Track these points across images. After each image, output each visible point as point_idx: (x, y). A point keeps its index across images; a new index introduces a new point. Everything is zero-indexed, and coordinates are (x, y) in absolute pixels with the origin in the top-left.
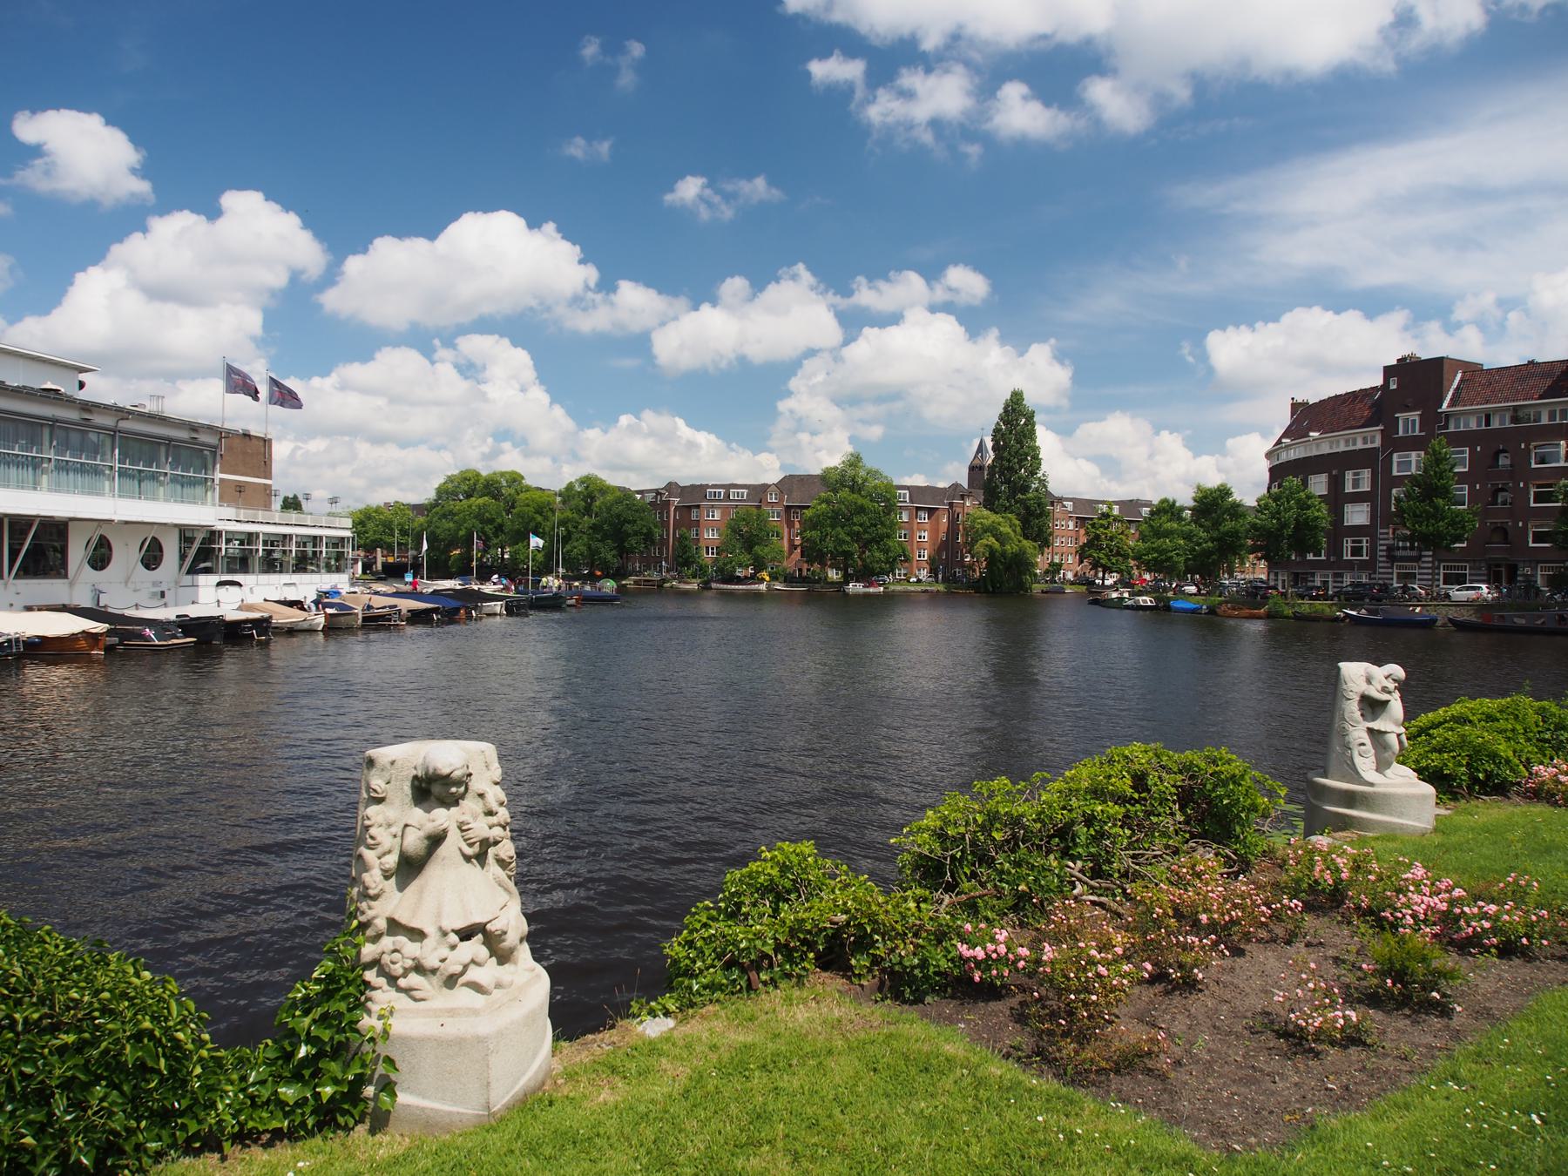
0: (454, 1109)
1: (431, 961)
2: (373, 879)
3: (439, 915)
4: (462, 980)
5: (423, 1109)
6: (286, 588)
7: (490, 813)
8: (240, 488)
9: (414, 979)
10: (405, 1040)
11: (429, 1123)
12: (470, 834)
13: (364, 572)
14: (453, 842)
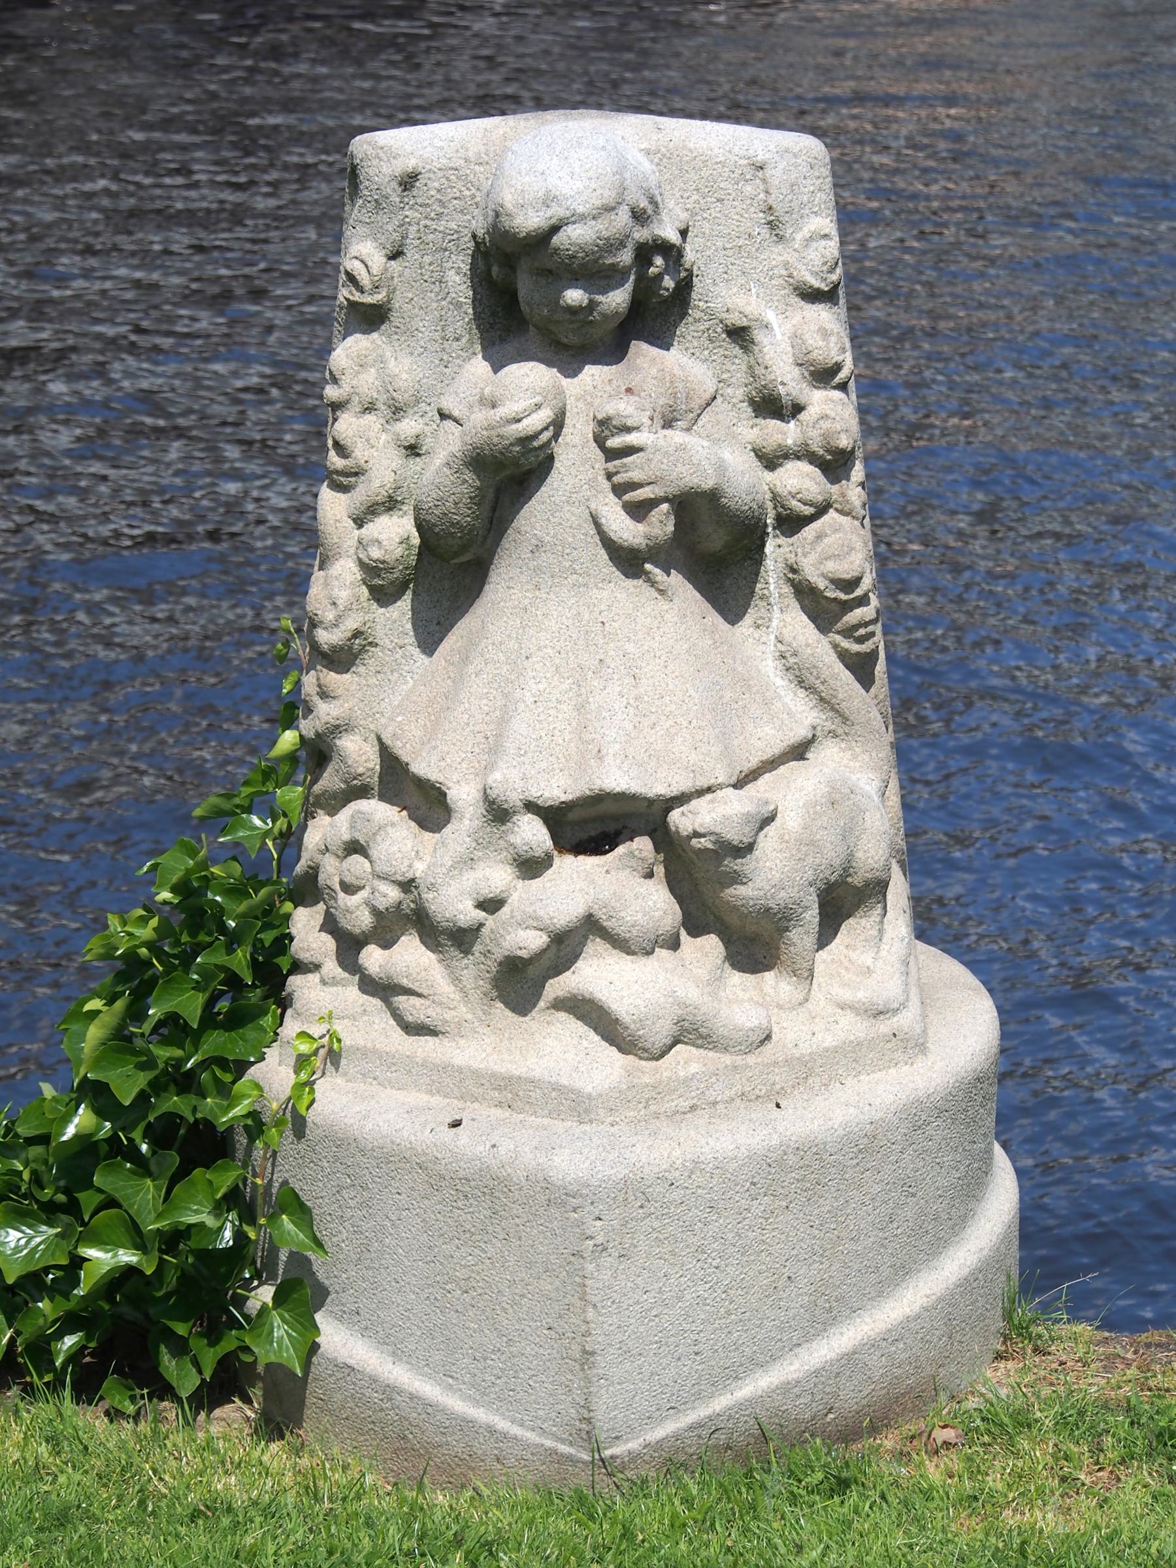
0: (481, 1415)
1: (454, 903)
2: (336, 594)
3: (494, 748)
4: (556, 987)
5: (390, 1390)
7: (770, 406)
9: (409, 957)
10: (344, 1146)
11: (413, 1447)
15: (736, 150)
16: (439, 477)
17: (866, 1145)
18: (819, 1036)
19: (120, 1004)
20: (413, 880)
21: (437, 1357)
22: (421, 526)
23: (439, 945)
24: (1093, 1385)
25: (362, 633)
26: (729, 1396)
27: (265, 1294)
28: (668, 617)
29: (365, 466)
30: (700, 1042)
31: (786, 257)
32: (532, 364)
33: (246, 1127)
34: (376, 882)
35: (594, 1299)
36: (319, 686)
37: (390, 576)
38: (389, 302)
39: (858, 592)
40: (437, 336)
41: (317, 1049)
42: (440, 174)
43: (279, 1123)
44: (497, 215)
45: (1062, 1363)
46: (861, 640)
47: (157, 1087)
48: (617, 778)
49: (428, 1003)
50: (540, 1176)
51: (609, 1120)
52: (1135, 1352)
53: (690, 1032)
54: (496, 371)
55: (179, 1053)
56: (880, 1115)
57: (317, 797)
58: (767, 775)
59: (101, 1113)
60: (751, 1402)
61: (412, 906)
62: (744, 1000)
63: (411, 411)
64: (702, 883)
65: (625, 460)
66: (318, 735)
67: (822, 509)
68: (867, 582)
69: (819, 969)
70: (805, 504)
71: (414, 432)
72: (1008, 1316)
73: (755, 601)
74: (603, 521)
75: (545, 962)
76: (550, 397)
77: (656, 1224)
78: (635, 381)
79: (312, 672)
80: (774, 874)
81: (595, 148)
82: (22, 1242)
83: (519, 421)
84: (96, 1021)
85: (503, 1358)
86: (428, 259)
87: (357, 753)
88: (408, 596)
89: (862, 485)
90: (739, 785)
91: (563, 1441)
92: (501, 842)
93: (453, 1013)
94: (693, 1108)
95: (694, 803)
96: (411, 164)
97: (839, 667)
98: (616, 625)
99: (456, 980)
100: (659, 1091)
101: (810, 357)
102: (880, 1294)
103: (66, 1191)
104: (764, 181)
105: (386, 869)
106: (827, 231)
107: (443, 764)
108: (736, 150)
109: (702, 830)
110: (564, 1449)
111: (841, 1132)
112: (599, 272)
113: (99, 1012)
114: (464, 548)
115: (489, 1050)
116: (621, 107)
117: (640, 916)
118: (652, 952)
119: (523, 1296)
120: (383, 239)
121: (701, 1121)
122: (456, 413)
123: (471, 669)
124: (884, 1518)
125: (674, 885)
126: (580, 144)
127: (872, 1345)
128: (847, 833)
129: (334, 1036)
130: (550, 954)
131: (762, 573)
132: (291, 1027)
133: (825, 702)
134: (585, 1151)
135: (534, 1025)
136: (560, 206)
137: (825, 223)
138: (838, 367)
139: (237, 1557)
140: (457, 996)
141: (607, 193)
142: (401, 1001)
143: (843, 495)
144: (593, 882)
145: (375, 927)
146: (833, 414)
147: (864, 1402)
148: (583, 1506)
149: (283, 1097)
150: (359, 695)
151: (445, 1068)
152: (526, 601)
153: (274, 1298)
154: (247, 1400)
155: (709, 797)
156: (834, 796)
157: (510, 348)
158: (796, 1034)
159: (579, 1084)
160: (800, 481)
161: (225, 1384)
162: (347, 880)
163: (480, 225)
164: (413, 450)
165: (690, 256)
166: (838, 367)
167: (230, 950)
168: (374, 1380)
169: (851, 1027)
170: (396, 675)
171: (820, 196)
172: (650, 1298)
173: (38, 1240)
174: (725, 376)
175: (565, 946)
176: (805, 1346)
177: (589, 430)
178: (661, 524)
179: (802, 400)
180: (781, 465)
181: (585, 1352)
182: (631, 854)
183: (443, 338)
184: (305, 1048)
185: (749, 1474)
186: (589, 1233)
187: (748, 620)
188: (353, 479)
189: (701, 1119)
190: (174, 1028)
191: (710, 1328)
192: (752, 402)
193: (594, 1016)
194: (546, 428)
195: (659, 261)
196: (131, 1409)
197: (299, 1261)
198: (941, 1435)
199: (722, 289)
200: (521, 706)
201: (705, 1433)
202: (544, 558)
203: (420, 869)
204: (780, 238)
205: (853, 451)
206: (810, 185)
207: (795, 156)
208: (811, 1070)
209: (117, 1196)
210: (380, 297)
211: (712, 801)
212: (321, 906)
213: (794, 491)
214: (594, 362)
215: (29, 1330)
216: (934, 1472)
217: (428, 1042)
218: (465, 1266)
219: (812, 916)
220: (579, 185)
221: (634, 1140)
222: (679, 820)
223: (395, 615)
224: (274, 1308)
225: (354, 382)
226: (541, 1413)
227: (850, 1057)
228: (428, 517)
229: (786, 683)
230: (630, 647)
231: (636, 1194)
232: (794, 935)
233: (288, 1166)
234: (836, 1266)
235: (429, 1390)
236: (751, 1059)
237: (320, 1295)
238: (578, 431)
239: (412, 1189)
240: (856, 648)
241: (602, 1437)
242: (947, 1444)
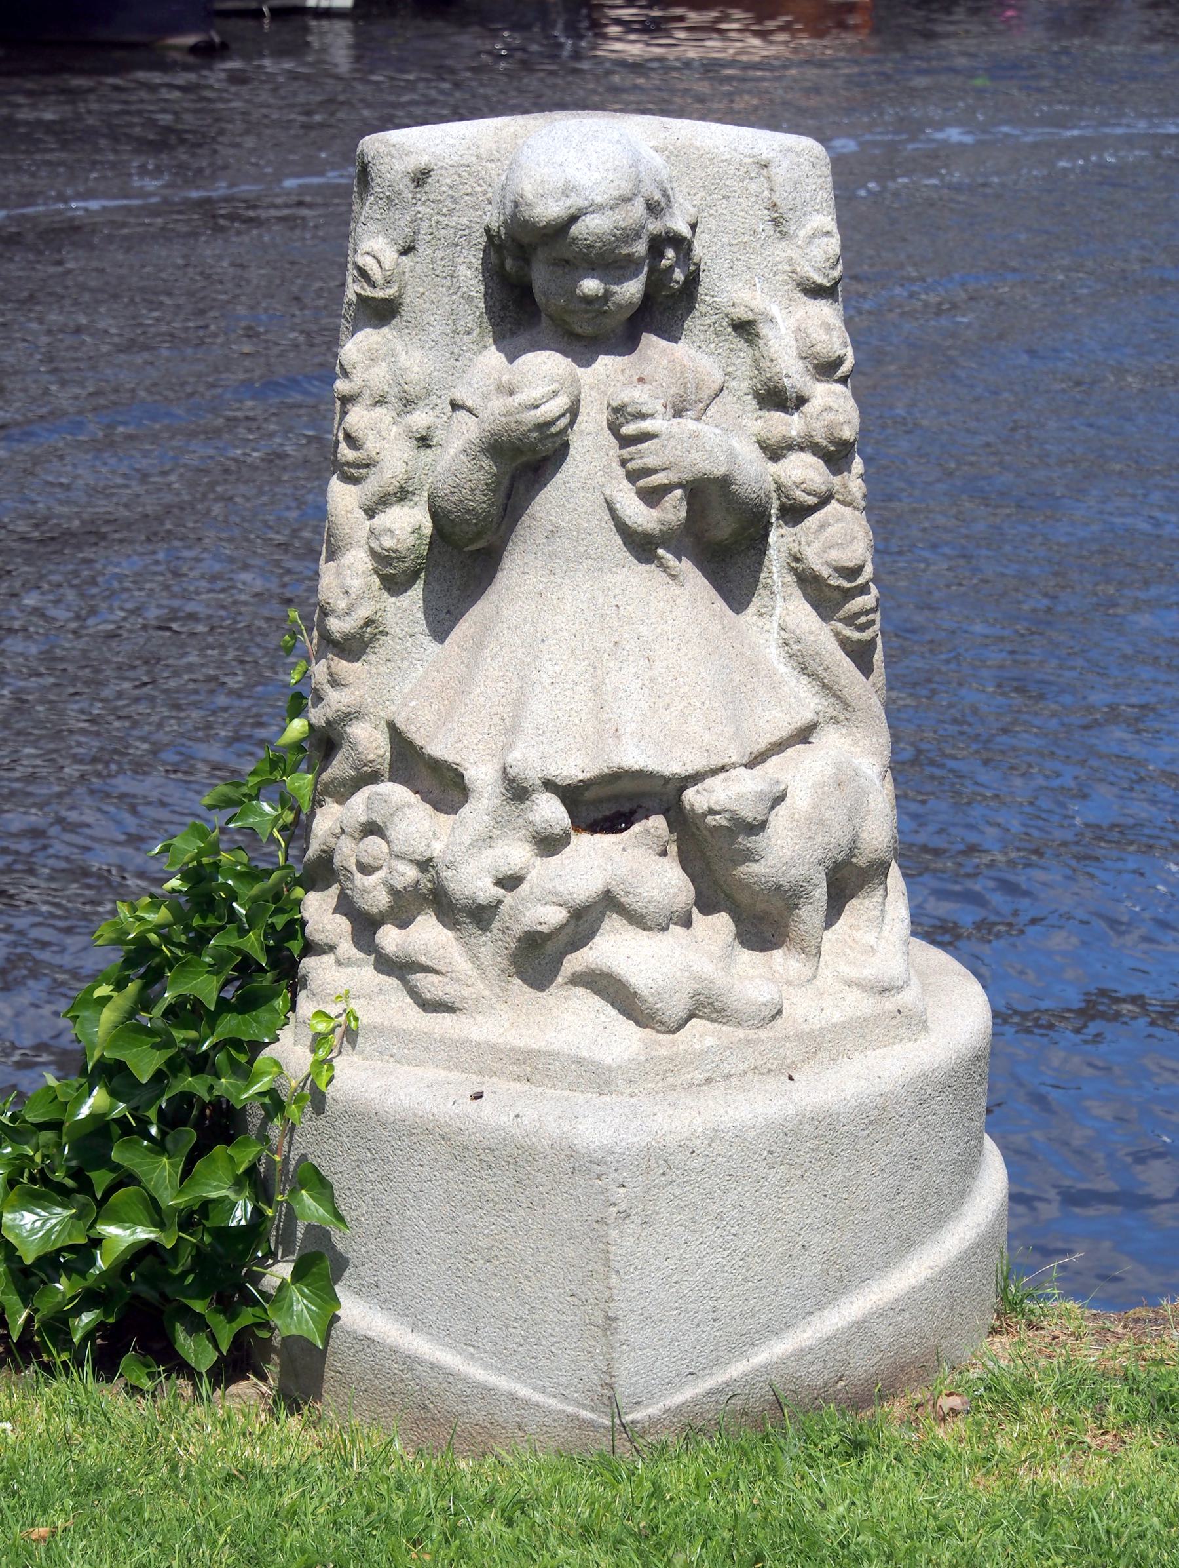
0: (503, 1383)
1: (473, 881)
3: (512, 730)
4: (574, 962)
5: (410, 1361)
7: (775, 398)
9: (426, 935)
10: (365, 1122)
11: (437, 1418)
14: (589, 473)
15: (741, 148)
16: (457, 463)
17: (876, 1117)
18: (828, 1012)
19: (132, 988)
20: (431, 860)
21: (459, 1326)
22: (436, 514)
23: (457, 922)
24: (1090, 1356)
25: (373, 621)
26: (745, 1362)
27: (283, 1270)
28: (679, 601)
29: (376, 458)
31: (790, 253)
32: (548, 353)
33: (263, 1105)
34: (394, 862)
35: (617, 1265)
36: (330, 674)
37: (402, 565)
38: (400, 296)
39: (861, 580)
40: (448, 330)
41: (334, 1029)
42: (452, 171)
43: (298, 1100)
44: (516, 205)
45: (1054, 1338)
46: (862, 628)
47: (173, 1067)
48: (634, 756)
49: (446, 980)
50: (565, 1144)
51: (628, 1091)
52: (1125, 1327)
53: (706, 1006)
54: (511, 361)
55: (193, 1034)
57: (326, 785)
58: (774, 758)
59: (114, 1094)
60: (766, 1368)
61: (429, 885)
62: (754, 976)
63: (422, 404)
64: (715, 859)
65: (640, 447)
66: (328, 722)
67: (825, 499)
68: (868, 571)
69: (825, 947)
71: (425, 424)
72: (1003, 1292)
73: (760, 590)
74: (618, 506)
75: (563, 938)
76: (567, 384)
77: (678, 1192)
78: (647, 370)
79: (323, 661)
80: (786, 852)
81: (610, 141)
82: (38, 1224)
83: (537, 407)
84: (110, 1005)
85: (525, 1326)
87: (368, 740)
88: (419, 586)
89: (861, 476)
90: (751, 764)
91: (585, 1407)
92: (520, 820)
93: (471, 990)
94: (708, 1081)
95: (709, 782)
96: (423, 160)
97: (841, 655)
98: (630, 608)
99: (474, 958)
100: (676, 1063)
101: (814, 350)
102: (887, 1265)
103: (83, 1171)
104: (768, 178)
105: (404, 849)
106: (829, 228)
107: (460, 745)
108: (741, 148)
109: (717, 808)
110: (585, 1414)
112: (615, 262)
113: (109, 998)
114: (479, 535)
115: (507, 1025)
116: (627, 109)
117: (656, 892)
119: (546, 1263)
121: (718, 1092)
122: (469, 403)
123: (487, 653)
124: (903, 1477)
126: (595, 138)
127: (881, 1314)
128: (854, 813)
129: (351, 1015)
130: (568, 930)
131: (766, 563)
132: (306, 1006)
133: (828, 689)
135: (552, 1001)
136: (579, 196)
137: (826, 220)
138: (840, 361)
139: (276, 1515)
140: (474, 973)
141: (624, 184)
142: (419, 979)
143: (845, 486)
144: (610, 858)
145: (392, 907)
146: (836, 406)
147: (873, 1370)
148: (607, 1467)
149: (302, 1076)
150: (370, 683)
151: (463, 1044)
152: (541, 586)
153: (294, 1274)
154: (263, 1378)
155: (722, 776)
156: (832, 782)
157: (521, 340)
158: (804, 1010)
159: (598, 1057)
160: (803, 471)
161: (238, 1363)
162: (365, 859)
163: (493, 218)
164: (424, 441)
165: (698, 251)
166: (840, 361)
167: (243, 933)
168: (394, 1351)
169: (859, 1004)
171: (822, 195)
172: (671, 1265)
173: (54, 1221)
174: (730, 369)
175: (584, 921)
176: (817, 1314)
177: (603, 417)
178: (674, 510)
179: (806, 392)
180: (785, 456)
182: (647, 832)
183: (454, 332)
184: (322, 1027)
185: (766, 1438)
186: (613, 1199)
187: (752, 609)
188: (364, 471)
189: (718, 1089)
190: (186, 1012)
192: (757, 395)
193: (611, 990)
194: (563, 415)
195: (670, 253)
196: (148, 1385)
197: (318, 1234)
198: (947, 1403)
199: (727, 284)
200: (538, 688)
201: (723, 1399)
202: (559, 544)
203: (437, 849)
204: (784, 235)
205: (853, 444)
206: (812, 184)
207: (798, 155)
208: (819, 1045)
209: (137, 1171)
210: (391, 291)
211: (726, 780)
212: (335, 890)
213: (798, 481)
214: (607, 353)
215: (46, 1306)
216: (944, 1435)
218: (487, 1236)
219: (820, 894)
220: (597, 176)
222: (693, 798)
223: (406, 604)
225: (365, 376)
226: (563, 1379)
228: (444, 504)
229: (789, 669)
230: (644, 630)
231: (659, 1161)
232: (803, 912)
233: (309, 1141)
234: (848, 1235)
235: (450, 1359)
236: (763, 1034)
237: (340, 1264)
238: (593, 419)
240: (857, 636)
241: (622, 1404)
242: (954, 1412)
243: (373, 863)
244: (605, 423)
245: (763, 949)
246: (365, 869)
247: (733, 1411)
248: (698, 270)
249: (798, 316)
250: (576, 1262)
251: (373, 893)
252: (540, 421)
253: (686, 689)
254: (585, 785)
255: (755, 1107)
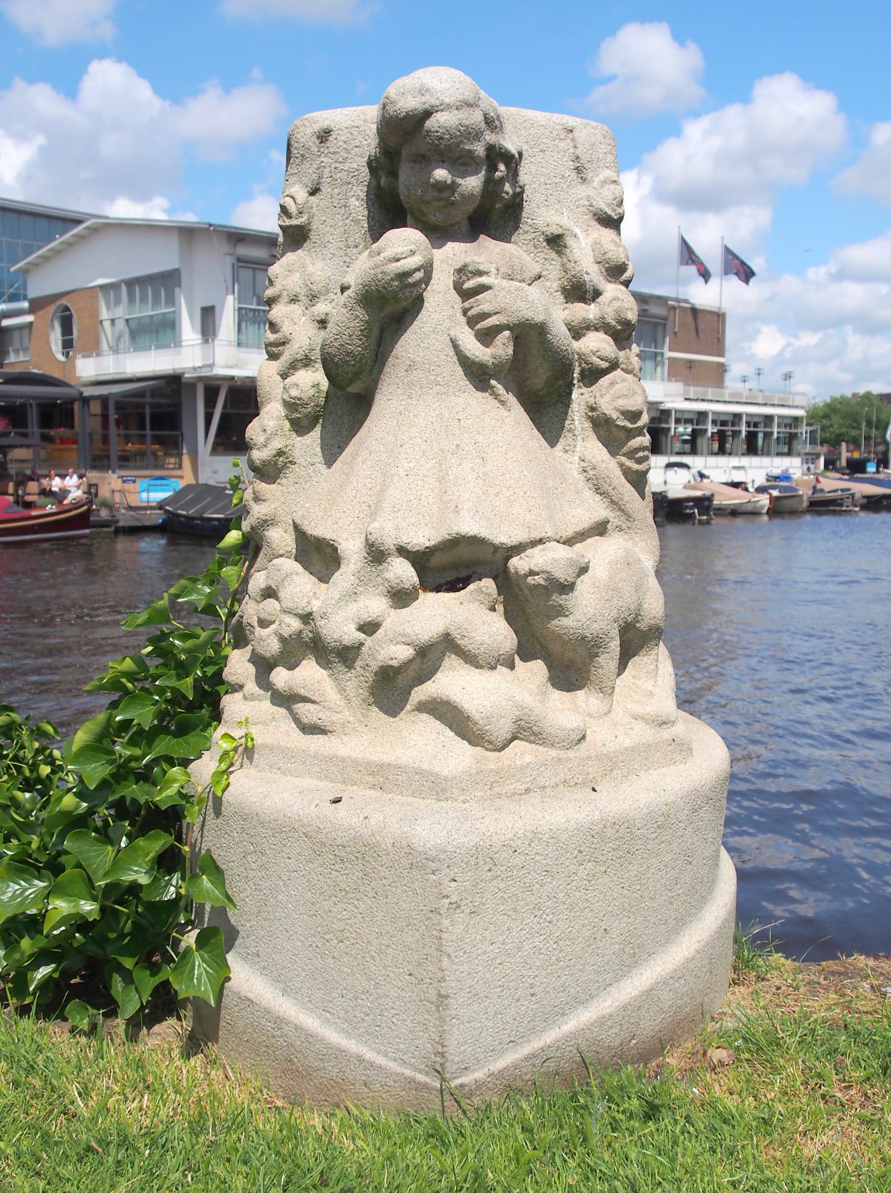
0: (352, 1045)
1: (341, 628)
4: (420, 694)
5: (280, 1021)
6: (734, 472)
8: (690, 365)
9: (309, 674)
10: (249, 819)
11: (297, 1071)
12: (484, 303)
13: (826, 467)
17: (661, 822)
18: (620, 738)
20: (310, 614)
25: (284, 453)
29: (289, 337)
30: (532, 738)
34: (283, 616)
35: (449, 950)
36: (254, 493)
37: (305, 411)
38: (309, 224)
39: (640, 423)
40: (342, 245)
42: (346, 131)
49: (319, 708)
53: (526, 731)
56: (672, 798)
58: (578, 545)
60: (575, 1034)
61: (311, 635)
62: (563, 710)
63: (322, 298)
64: (533, 612)
65: (478, 297)
67: (614, 365)
70: (602, 360)
73: (565, 433)
74: (460, 343)
75: (411, 672)
77: (502, 885)
80: (589, 610)
83: (398, 260)
85: (371, 998)
86: (336, 191)
88: (318, 428)
91: (420, 1071)
92: (379, 579)
94: (527, 791)
98: (469, 422)
99: (342, 690)
104: (573, 140)
105: (290, 605)
109: (536, 569)
110: (421, 1078)
111: (645, 811)
115: (366, 744)
117: (486, 637)
118: (495, 668)
119: (388, 946)
120: (305, 180)
123: (359, 459)
125: (509, 618)
127: (664, 982)
130: (415, 666)
131: (570, 413)
134: (443, 822)
135: (402, 725)
136: (432, 96)
140: (342, 703)
141: (467, 93)
142: (300, 707)
145: (282, 652)
146: (622, 297)
147: (657, 1029)
150: (282, 499)
151: (331, 759)
152: (402, 408)
155: (540, 547)
158: (604, 736)
159: (436, 770)
161: (165, 1003)
168: (268, 1011)
169: (643, 733)
170: (308, 484)
173: (30, 891)
175: (430, 656)
176: (615, 985)
178: (502, 348)
180: (584, 335)
181: (440, 995)
182: (480, 590)
185: (574, 1098)
186: (445, 892)
187: (559, 447)
191: (544, 973)
193: (449, 716)
194: (418, 269)
199: (543, 211)
201: (538, 1062)
202: (416, 375)
203: (316, 606)
204: (584, 180)
208: (614, 764)
210: (302, 220)
213: (595, 349)
217: (319, 739)
219: (615, 645)
221: (483, 814)
222: (518, 564)
224: (197, 951)
225: (284, 283)
226: (402, 1046)
227: (642, 756)
228: (330, 350)
230: (480, 438)
231: (486, 859)
232: (602, 659)
233: (207, 836)
234: (640, 919)
235: (311, 1022)
236: (571, 754)
237: (232, 935)
239: (299, 854)
240: (635, 467)
243: (268, 618)
244: (451, 285)
245: (569, 690)
246: (264, 623)
247: (547, 1074)
248: (523, 192)
249: (594, 236)
250: (413, 946)
251: (268, 642)
252: (400, 271)
253: (512, 482)
254: (430, 552)
255: (565, 813)
